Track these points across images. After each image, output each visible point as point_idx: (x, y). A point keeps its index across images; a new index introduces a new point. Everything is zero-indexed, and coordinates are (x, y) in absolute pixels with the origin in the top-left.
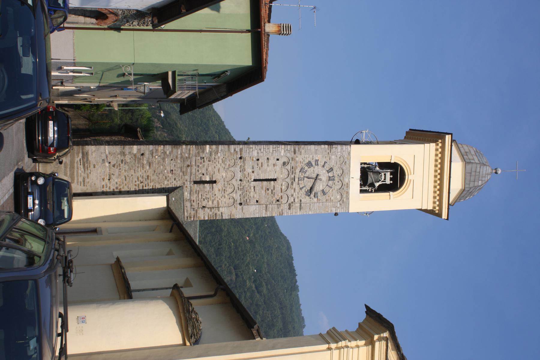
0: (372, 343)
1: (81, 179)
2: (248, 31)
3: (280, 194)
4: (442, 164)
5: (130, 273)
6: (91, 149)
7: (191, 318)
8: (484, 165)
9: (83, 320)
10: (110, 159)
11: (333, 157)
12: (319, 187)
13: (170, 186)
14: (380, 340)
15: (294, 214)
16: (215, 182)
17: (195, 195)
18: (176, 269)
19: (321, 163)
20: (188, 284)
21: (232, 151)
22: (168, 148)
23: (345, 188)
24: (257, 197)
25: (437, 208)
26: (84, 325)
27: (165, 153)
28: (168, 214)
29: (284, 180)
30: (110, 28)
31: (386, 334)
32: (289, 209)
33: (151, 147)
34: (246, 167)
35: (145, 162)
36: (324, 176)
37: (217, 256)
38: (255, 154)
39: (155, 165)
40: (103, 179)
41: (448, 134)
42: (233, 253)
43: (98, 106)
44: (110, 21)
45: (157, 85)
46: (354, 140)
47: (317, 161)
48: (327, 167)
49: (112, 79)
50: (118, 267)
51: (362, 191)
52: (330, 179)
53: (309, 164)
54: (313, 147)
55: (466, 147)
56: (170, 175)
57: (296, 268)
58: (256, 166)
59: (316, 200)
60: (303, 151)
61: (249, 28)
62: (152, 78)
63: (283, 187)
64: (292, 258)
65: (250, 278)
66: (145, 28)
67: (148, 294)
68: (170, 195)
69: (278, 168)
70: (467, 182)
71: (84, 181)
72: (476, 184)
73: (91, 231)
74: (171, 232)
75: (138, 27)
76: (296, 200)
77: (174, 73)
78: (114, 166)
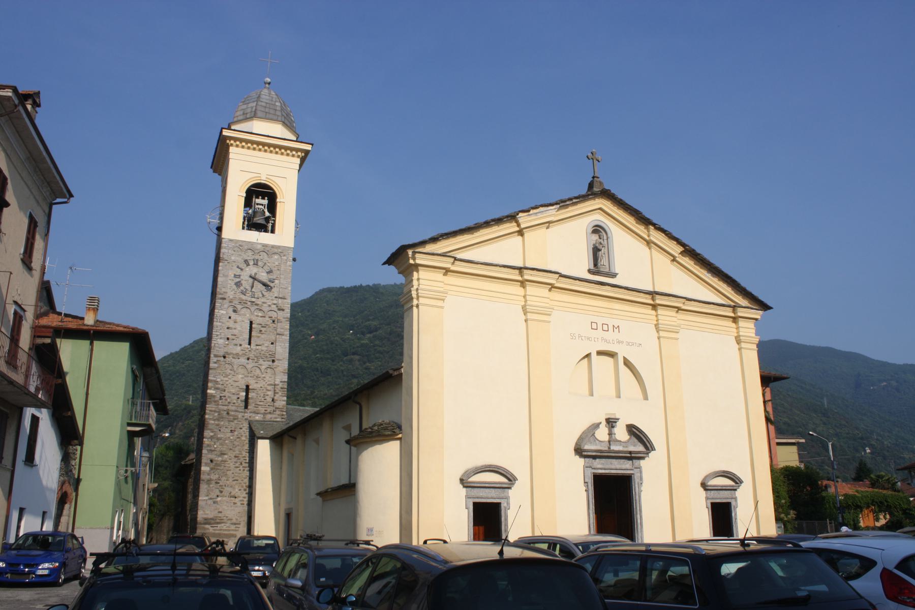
0: (416, 267)
1: (233, 527)
2: (92, 344)
3: (267, 319)
4: (253, 142)
5: (332, 483)
6: (201, 515)
7: (378, 431)
8: (259, 97)
9: (370, 530)
10: (213, 495)
11: (233, 258)
12: (263, 276)
13: (248, 434)
14: (414, 259)
15: (288, 291)
16: (247, 386)
17: (260, 408)
18: (333, 437)
19: (238, 272)
20: (348, 428)
21: (216, 365)
22: (207, 433)
23: (268, 249)
24: (267, 343)
25: (299, 153)
26: (374, 530)
27: (211, 438)
28: (277, 440)
29: (252, 313)
30: (76, 490)
31: (410, 252)
32: (283, 310)
33: (204, 451)
34: (234, 352)
35: (220, 459)
36: (252, 270)
37: (330, 375)
38: (221, 341)
39: (224, 449)
40: (235, 503)
41: (221, 132)
42: (328, 356)
43: (151, 505)
44: (69, 489)
45: (138, 442)
46: (216, 232)
47: (235, 276)
48: (243, 266)
49: (128, 489)
50: (325, 495)
51: (273, 231)
52: (256, 264)
53: (238, 284)
54: (220, 279)
55: (238, 113)
56: (236, 433)
57: (353, 284)
58: (234, 342)
59: (277, 281)
60: (224, 290)
61: (88, 342)
62: (131, 447)
63: (260, 314)
64: (341, 288)
65: (359, 339)
66: (79, 452)
67: (353, 468)
68: (258, 435)
69: (239, 318)
70: (275, 118)
71: (235, 524)
72: (279, 108)
73: (287, 519)
74: (295, 438)
75: (78, 460)
76: (275, 302)
77: (129, 424)
78: (221, 492)
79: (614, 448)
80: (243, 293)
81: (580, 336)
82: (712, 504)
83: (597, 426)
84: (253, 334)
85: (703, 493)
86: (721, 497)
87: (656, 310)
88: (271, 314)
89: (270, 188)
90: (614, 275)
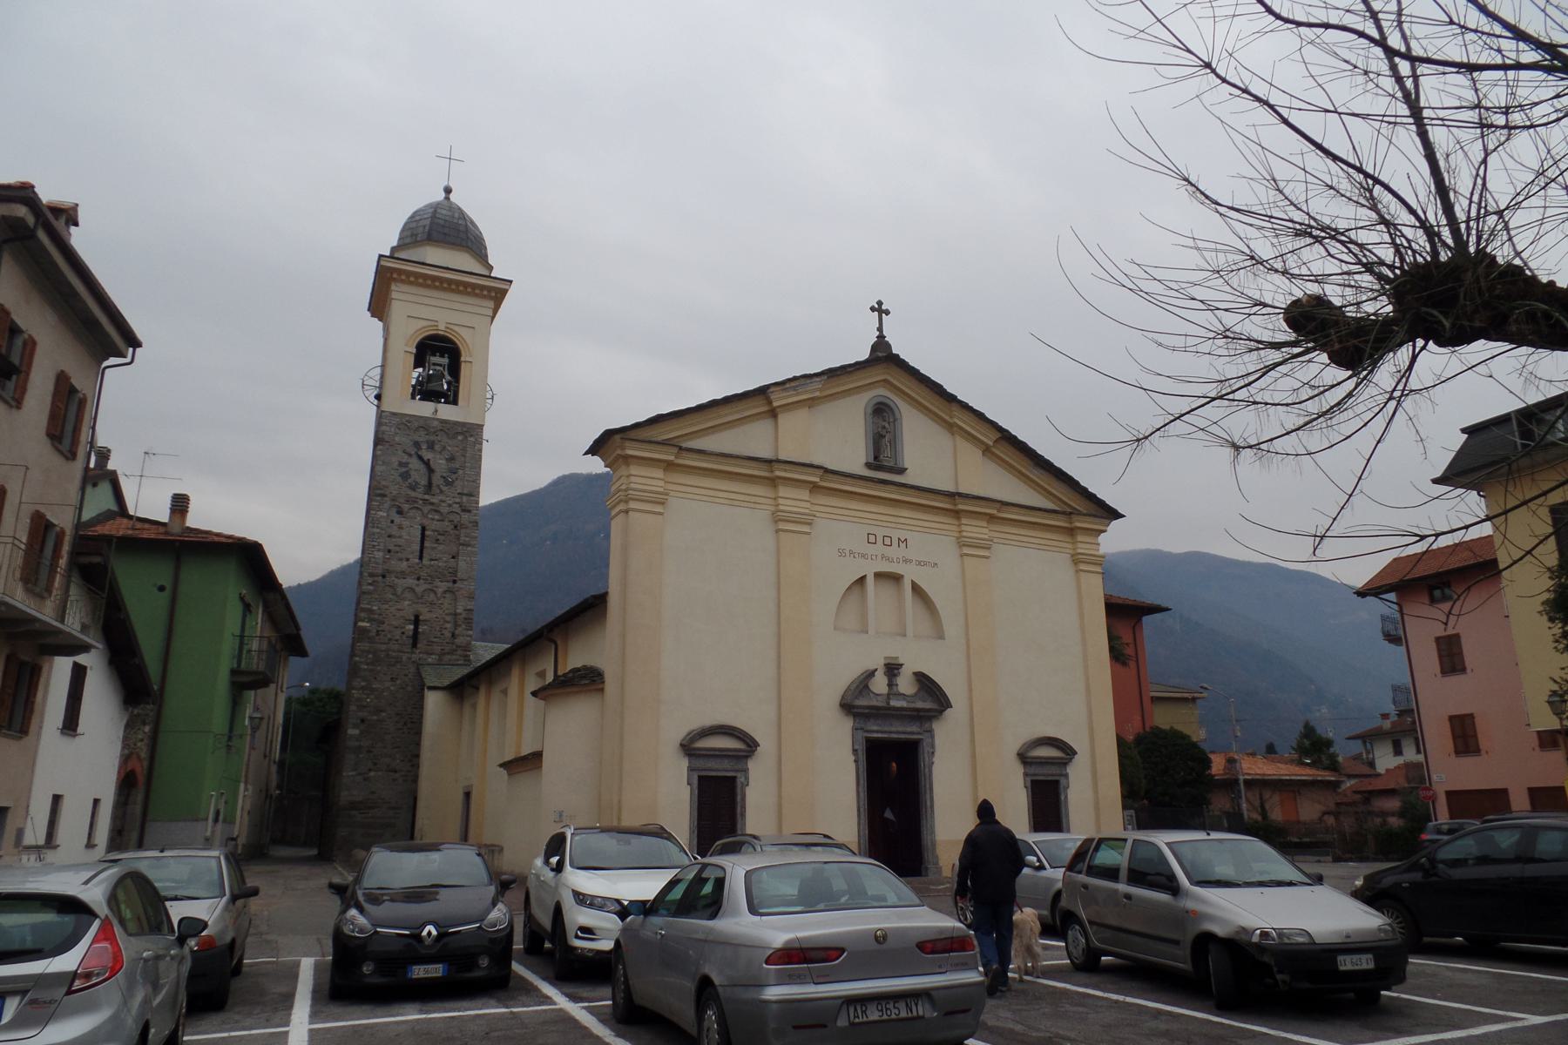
16: (417, 617)
19: (405, 459)
20: (542, 674)
29: (425, 516)
47: (401, 464)
69: (406, 523)
79: (894, 703)
80: (413, 488)
81: (851, 552)
82: (868, 740)
83: (872, 674)
84: (427, 544)
85: (847, 724)
86: (1044, 773)
87: (959, 518)
88: (452, 517)
89: (453, 343)
90: (902, 471)
